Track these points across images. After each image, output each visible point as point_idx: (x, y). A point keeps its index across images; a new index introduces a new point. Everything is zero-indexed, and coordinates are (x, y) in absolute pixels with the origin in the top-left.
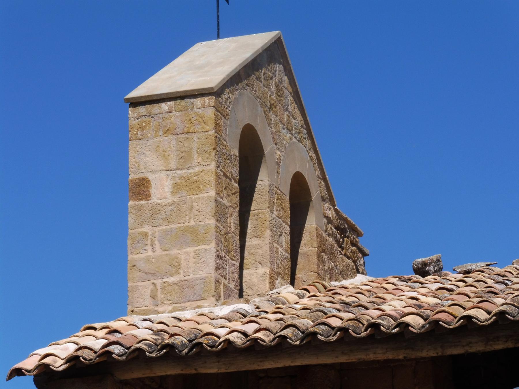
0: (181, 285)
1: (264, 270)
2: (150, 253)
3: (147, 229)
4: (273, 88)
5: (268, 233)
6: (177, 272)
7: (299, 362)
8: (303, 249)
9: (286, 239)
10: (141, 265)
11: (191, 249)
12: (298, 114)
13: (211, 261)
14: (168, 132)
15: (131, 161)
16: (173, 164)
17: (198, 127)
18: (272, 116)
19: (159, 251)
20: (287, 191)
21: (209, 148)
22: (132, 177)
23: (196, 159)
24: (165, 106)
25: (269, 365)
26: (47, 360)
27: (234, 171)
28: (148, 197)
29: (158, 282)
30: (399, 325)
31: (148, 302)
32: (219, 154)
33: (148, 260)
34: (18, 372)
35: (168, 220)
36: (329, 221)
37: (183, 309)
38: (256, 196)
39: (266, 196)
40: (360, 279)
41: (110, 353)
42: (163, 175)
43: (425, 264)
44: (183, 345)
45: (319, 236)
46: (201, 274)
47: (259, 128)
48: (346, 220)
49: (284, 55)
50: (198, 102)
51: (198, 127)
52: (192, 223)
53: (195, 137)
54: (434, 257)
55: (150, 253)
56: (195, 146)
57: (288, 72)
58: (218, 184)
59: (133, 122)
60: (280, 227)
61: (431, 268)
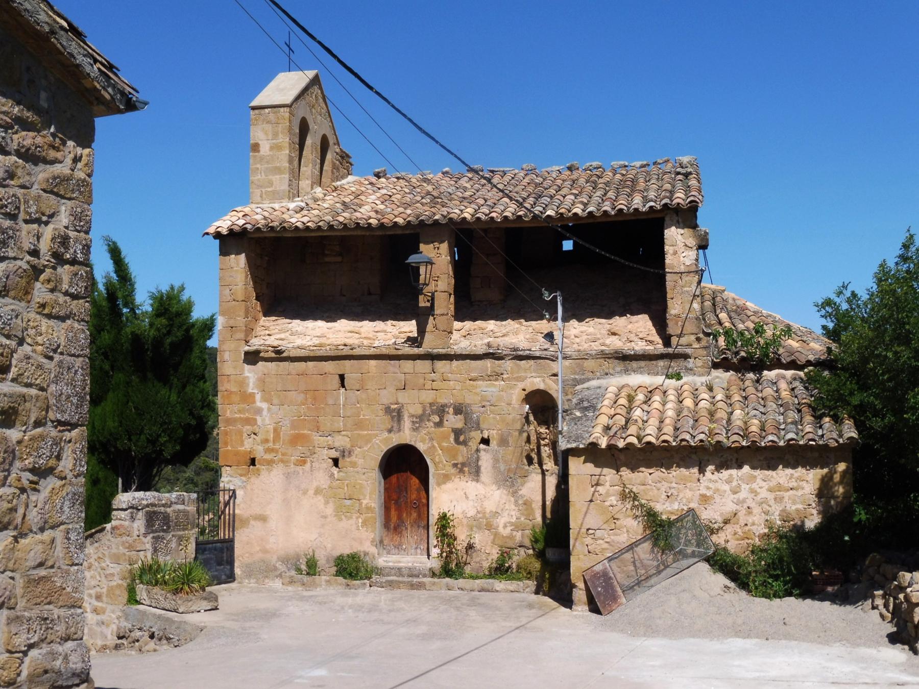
0: (274, 192)
1: (309, 182)
2: (259, 177)
3: (258, 166)
4: (314, 97)
5: (311, 165)
6: (272, 186)
7: (325, 234)
8: (325, 168)
9: (318, 166)
10: (256, 182)
11: (278, 177)
12: (324, 106)
13: (287, 182)
14: (268, 122)
15: (251, 134)
16: (270, 137)
17: (282, 121)
18: (313, 110)
19: (264, 176)
20: (319, 144)
21: (286, 131)
22: (252, 142)
23: (281, 136)
24: (267, 111)
25: (313, 234)
26: (219, 229)
27: (297, 140)
28: (259, 151)
29: (263, 190)
30: (368, 223)
31: (259, 199)
32: (290, 134)
33: (258, 180)
34: (207, 234)
35: (268, 162)
36: (337, 154)
37: (274, 203)
38: (305, 148)
39: (310, 148)
40: (350, 178)
41: (246, 228)
42: (265, 142)
43: (379, 173)
44: (278, 227)
45: (332, 161)
46: (282, 188)
47: (307, 118)
48: (345, 152)
49: (319, 81)
50: (282, 110)
51: (282, 121)
52: (278, 165)
53: (280, 125)
54: (383, 169)
55: (259, 177)
56: (280, 129)
57: (321, 88)
58: (290, 147)
59: (252, 117)
60: (316, 161)
61: (382, 175)
